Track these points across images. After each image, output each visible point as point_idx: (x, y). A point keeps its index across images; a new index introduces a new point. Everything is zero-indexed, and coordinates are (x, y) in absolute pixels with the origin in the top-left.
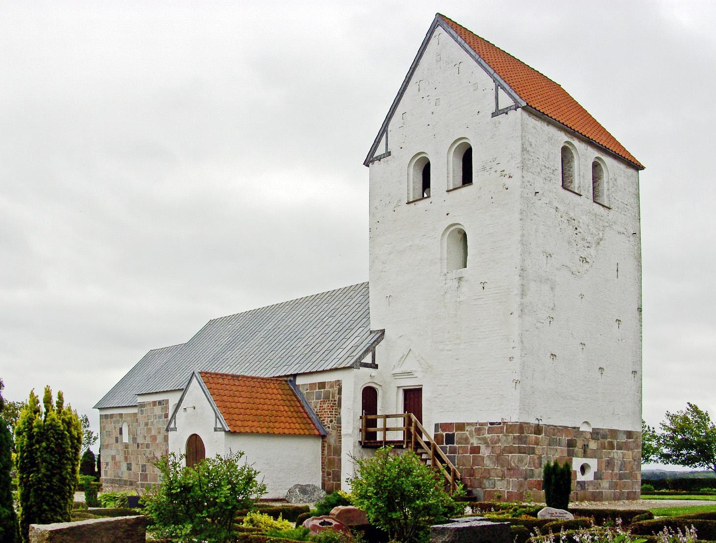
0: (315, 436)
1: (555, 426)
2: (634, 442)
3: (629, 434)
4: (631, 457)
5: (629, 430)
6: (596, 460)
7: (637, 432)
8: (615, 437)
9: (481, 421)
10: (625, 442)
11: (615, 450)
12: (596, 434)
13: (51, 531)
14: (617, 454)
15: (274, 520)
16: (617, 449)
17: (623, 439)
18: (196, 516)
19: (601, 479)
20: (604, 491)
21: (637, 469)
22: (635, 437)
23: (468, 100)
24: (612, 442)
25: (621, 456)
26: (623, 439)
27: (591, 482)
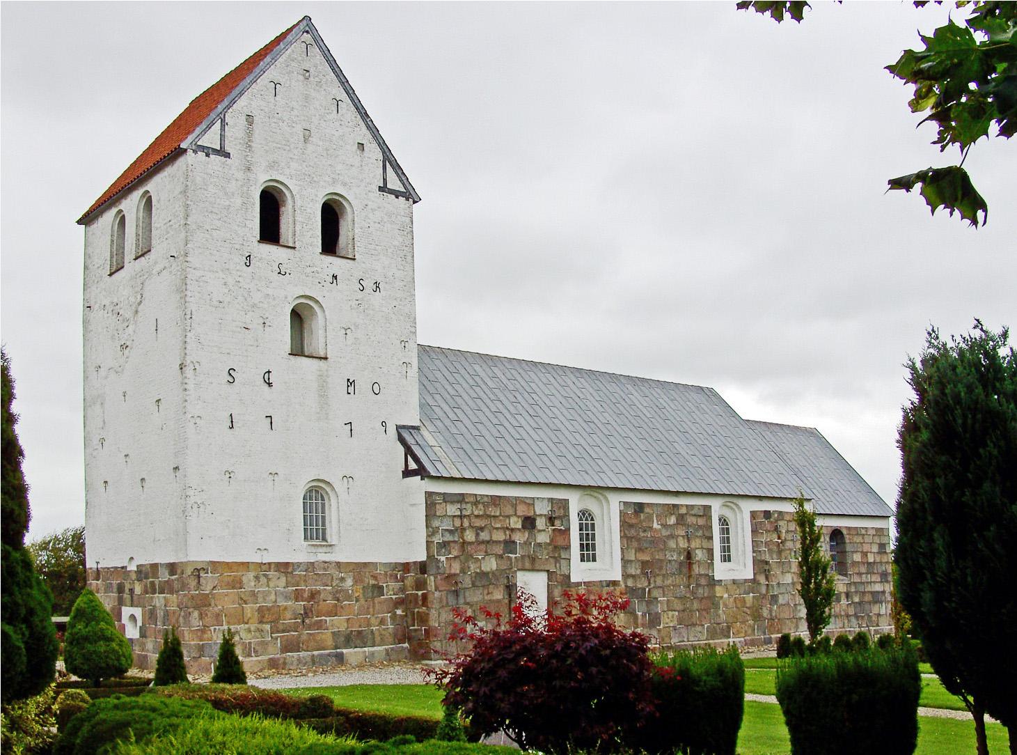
0: (544, 571)
1: (108, 568)
2: (177, 579)
3: (172, 568)
4: (175, 604)
5: (172, 562)
6: (140, 609)
7: (182, 563)
8: (155, 575)
9: (108, 566)
10: (167, 581)
11: (157, 595)
12: (142, 573)
13: (109, 697)
14: (159, 600)
15: (644, 640)
16: (159, 593)
17: (164, 576)
18: (599, 643)
19: (146, 637)
20: (148, 654)
21: (184, 623)
22: (179, 571)
23: (247, 117)
24: (153, 582)
25: (163, 602)
26: (164, 576)
27: (138, 639)
